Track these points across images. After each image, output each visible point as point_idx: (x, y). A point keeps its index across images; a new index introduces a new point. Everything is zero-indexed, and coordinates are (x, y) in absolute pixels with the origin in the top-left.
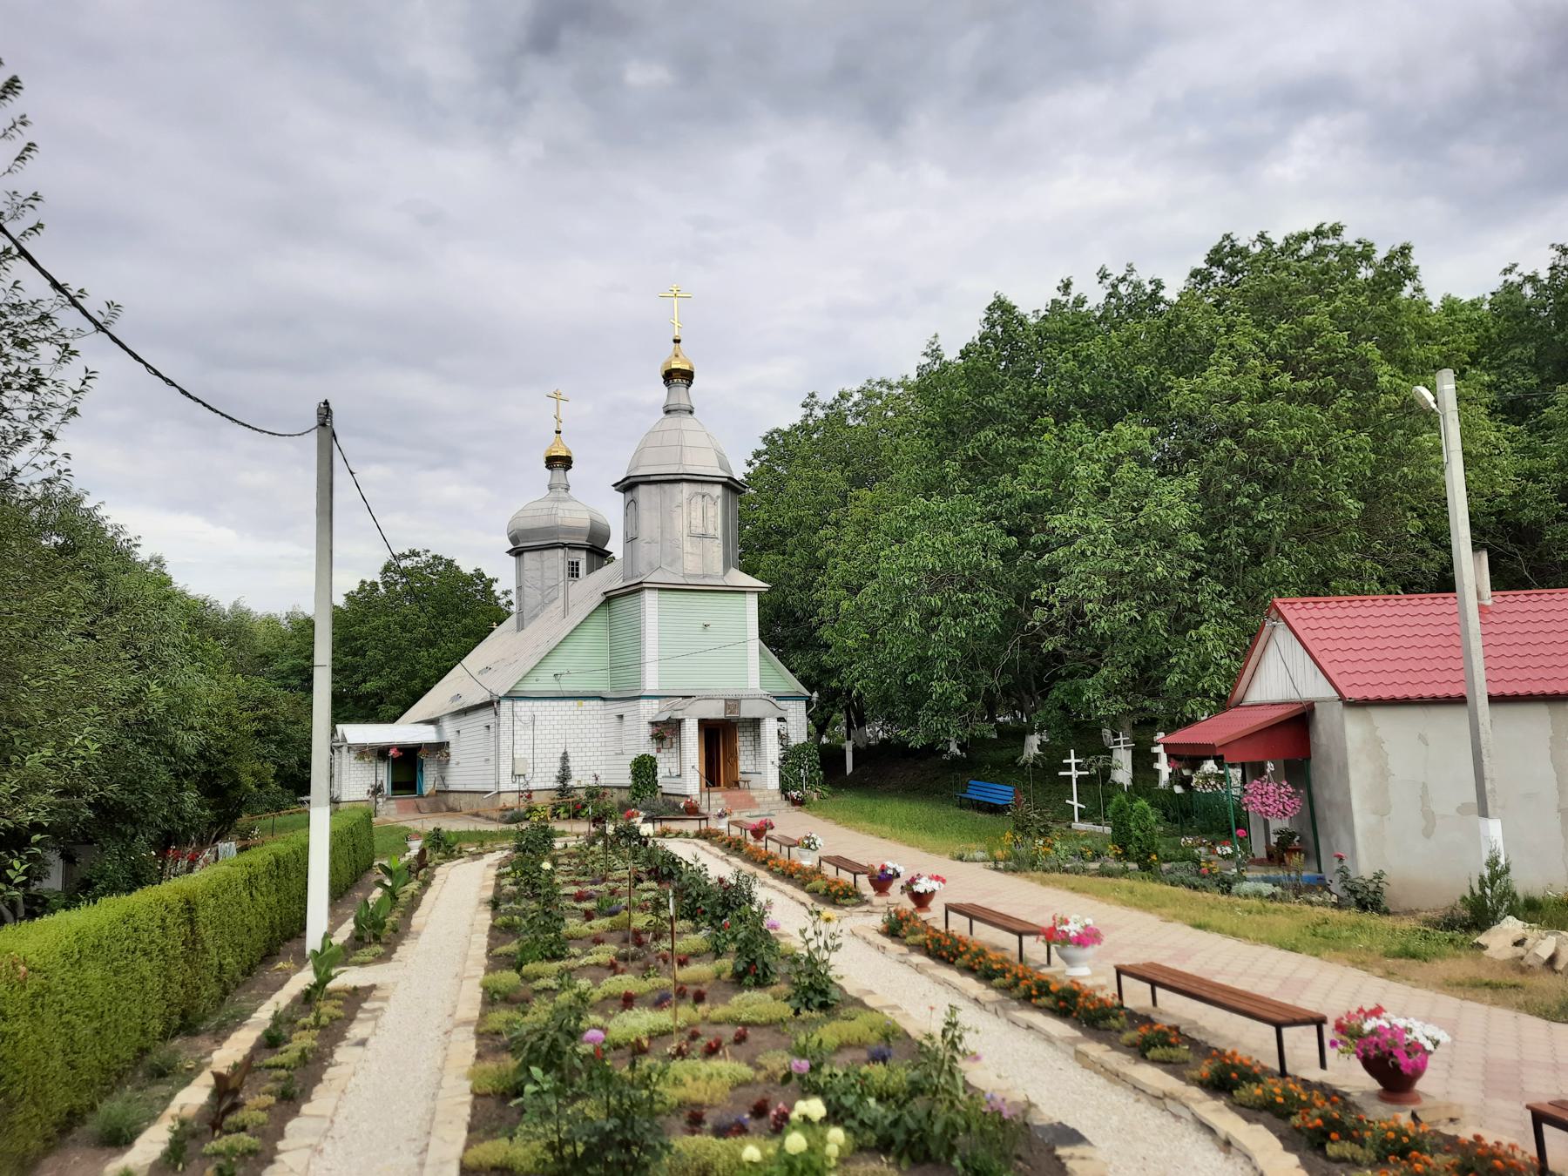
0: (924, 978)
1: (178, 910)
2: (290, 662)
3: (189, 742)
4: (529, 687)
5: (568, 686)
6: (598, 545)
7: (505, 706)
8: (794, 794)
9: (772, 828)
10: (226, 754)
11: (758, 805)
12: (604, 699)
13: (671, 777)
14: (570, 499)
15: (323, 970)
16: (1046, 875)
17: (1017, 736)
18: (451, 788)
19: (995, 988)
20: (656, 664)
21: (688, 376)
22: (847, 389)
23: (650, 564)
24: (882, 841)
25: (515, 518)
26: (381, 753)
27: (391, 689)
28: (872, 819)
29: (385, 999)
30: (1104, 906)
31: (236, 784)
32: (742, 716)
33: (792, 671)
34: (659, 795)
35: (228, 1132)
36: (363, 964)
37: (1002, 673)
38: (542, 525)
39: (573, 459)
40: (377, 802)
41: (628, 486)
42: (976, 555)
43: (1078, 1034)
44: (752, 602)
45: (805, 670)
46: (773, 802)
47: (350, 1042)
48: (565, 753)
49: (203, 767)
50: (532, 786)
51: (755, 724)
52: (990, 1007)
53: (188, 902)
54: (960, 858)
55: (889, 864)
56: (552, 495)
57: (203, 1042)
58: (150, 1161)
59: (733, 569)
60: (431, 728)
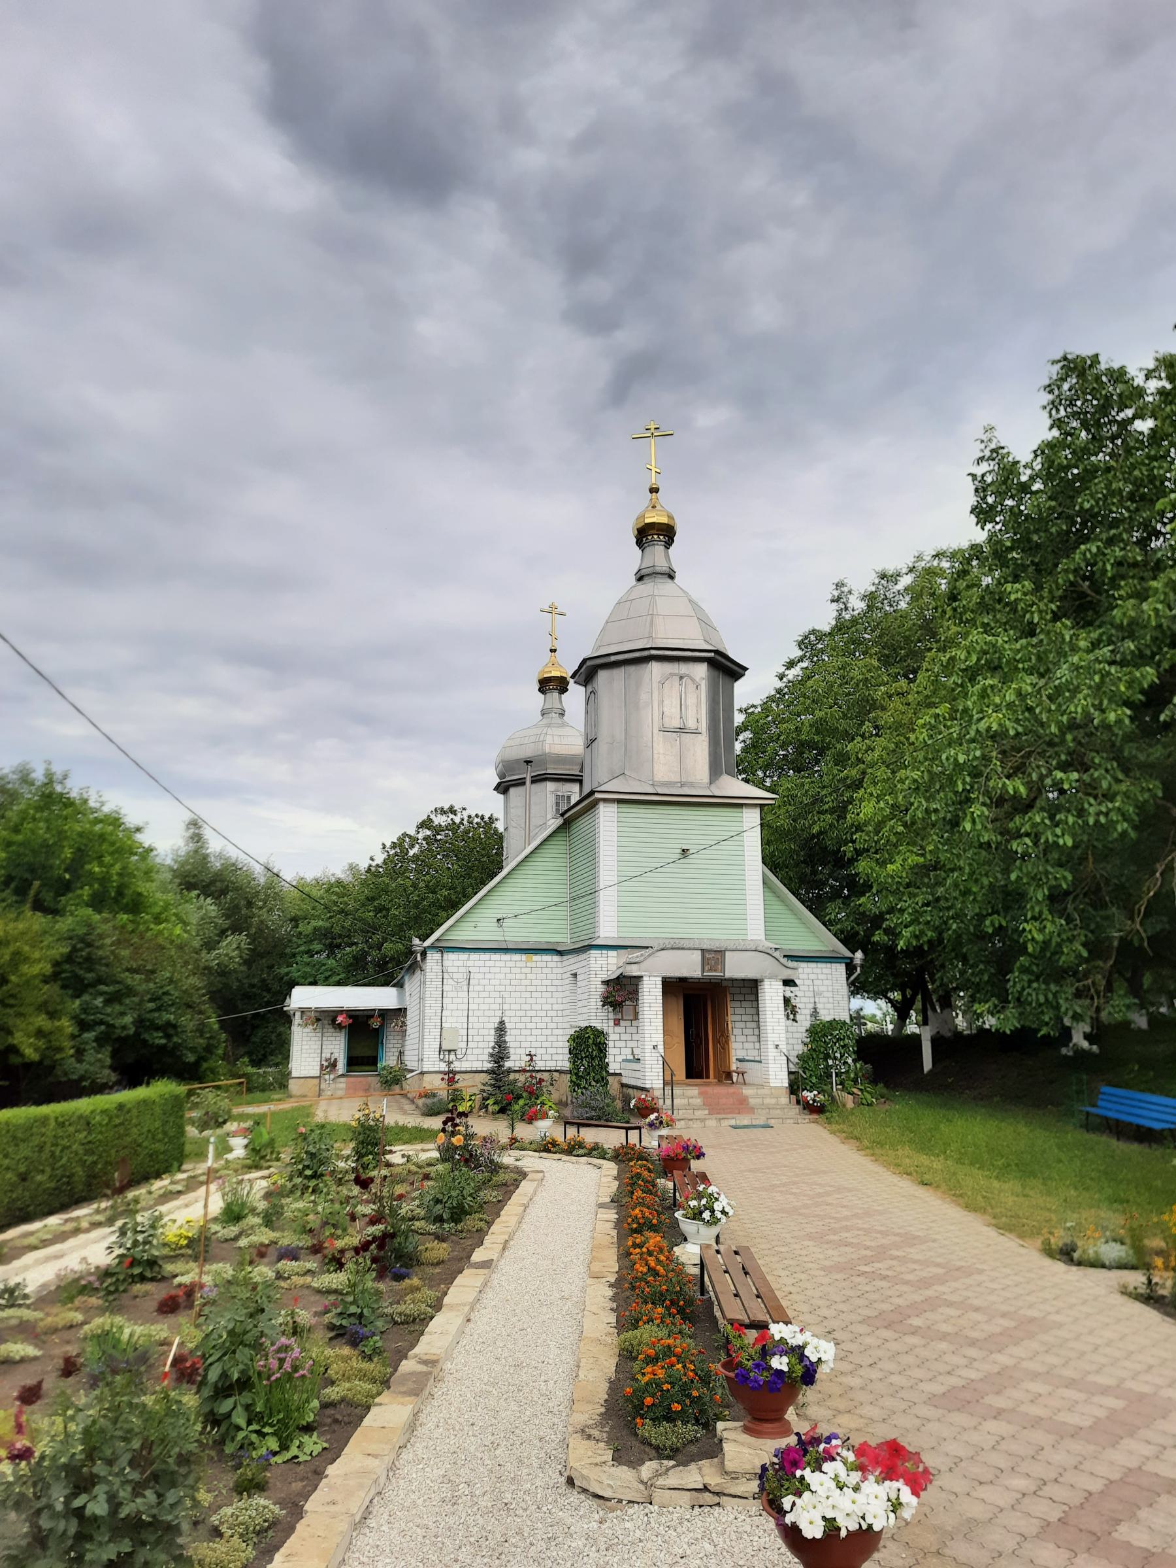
5: (516, 933)
8: (809, 1095)
9: (700, 1155)
11: (751, 1110)
12: (560, 953)
14: (564, 725)
22: (891, 569)
28: (925, 1145)
32: (728, 975)
37: (1148, 914)
42: (1080, 705)
44: (752, 818)
48: (502, 1023)
50: (457, 1066)
51: (750, 988)
54: (1067, 1254)
56: (545, 721)
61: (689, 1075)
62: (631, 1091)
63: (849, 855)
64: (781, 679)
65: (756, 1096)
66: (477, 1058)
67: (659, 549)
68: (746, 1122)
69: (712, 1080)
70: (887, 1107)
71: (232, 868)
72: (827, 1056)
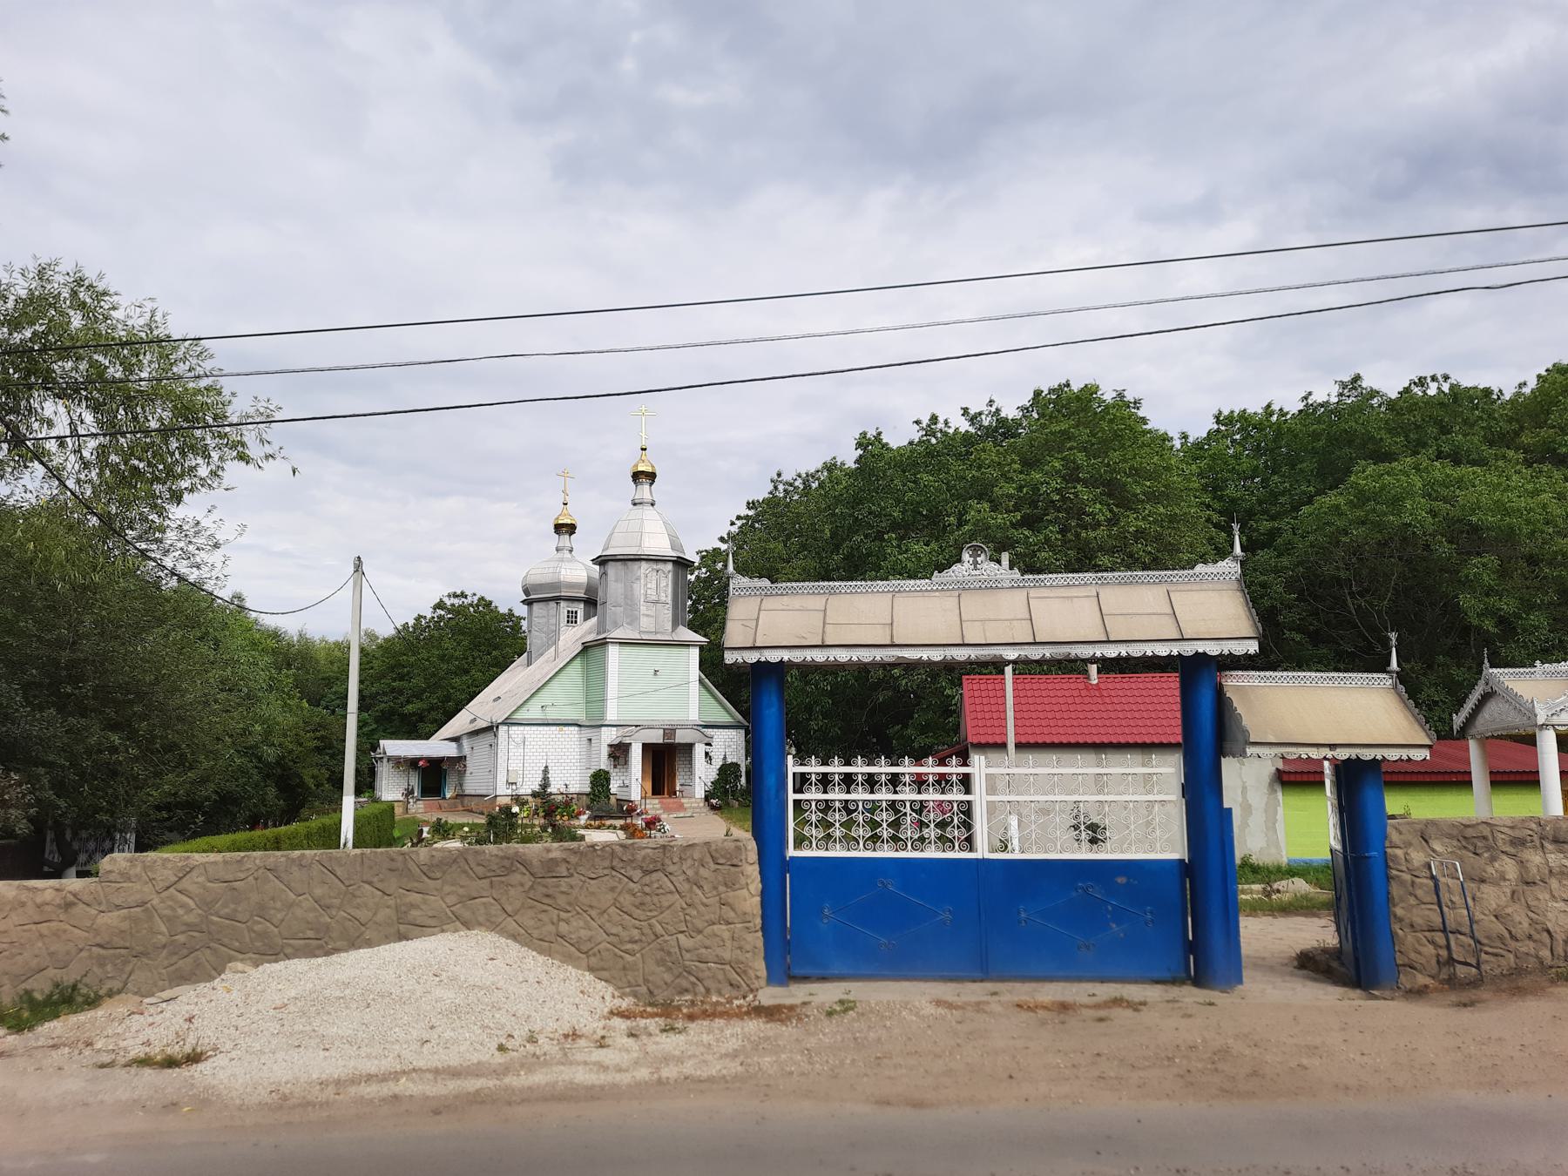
3: (270, 753)
5: (552, 715)
7: (503, 729)
8: (714, 801)
18: (467, 792)
21: (651, 476)
26: (413, 763)
38: (548, 581)
41: (602, 561)
46: (698, 807)
48: (546, 767)
51: (688, 748)
59: (681, 627)
60: (454, 745)
61: (653, 794)
67: (647, 487)
69: (666, 796)
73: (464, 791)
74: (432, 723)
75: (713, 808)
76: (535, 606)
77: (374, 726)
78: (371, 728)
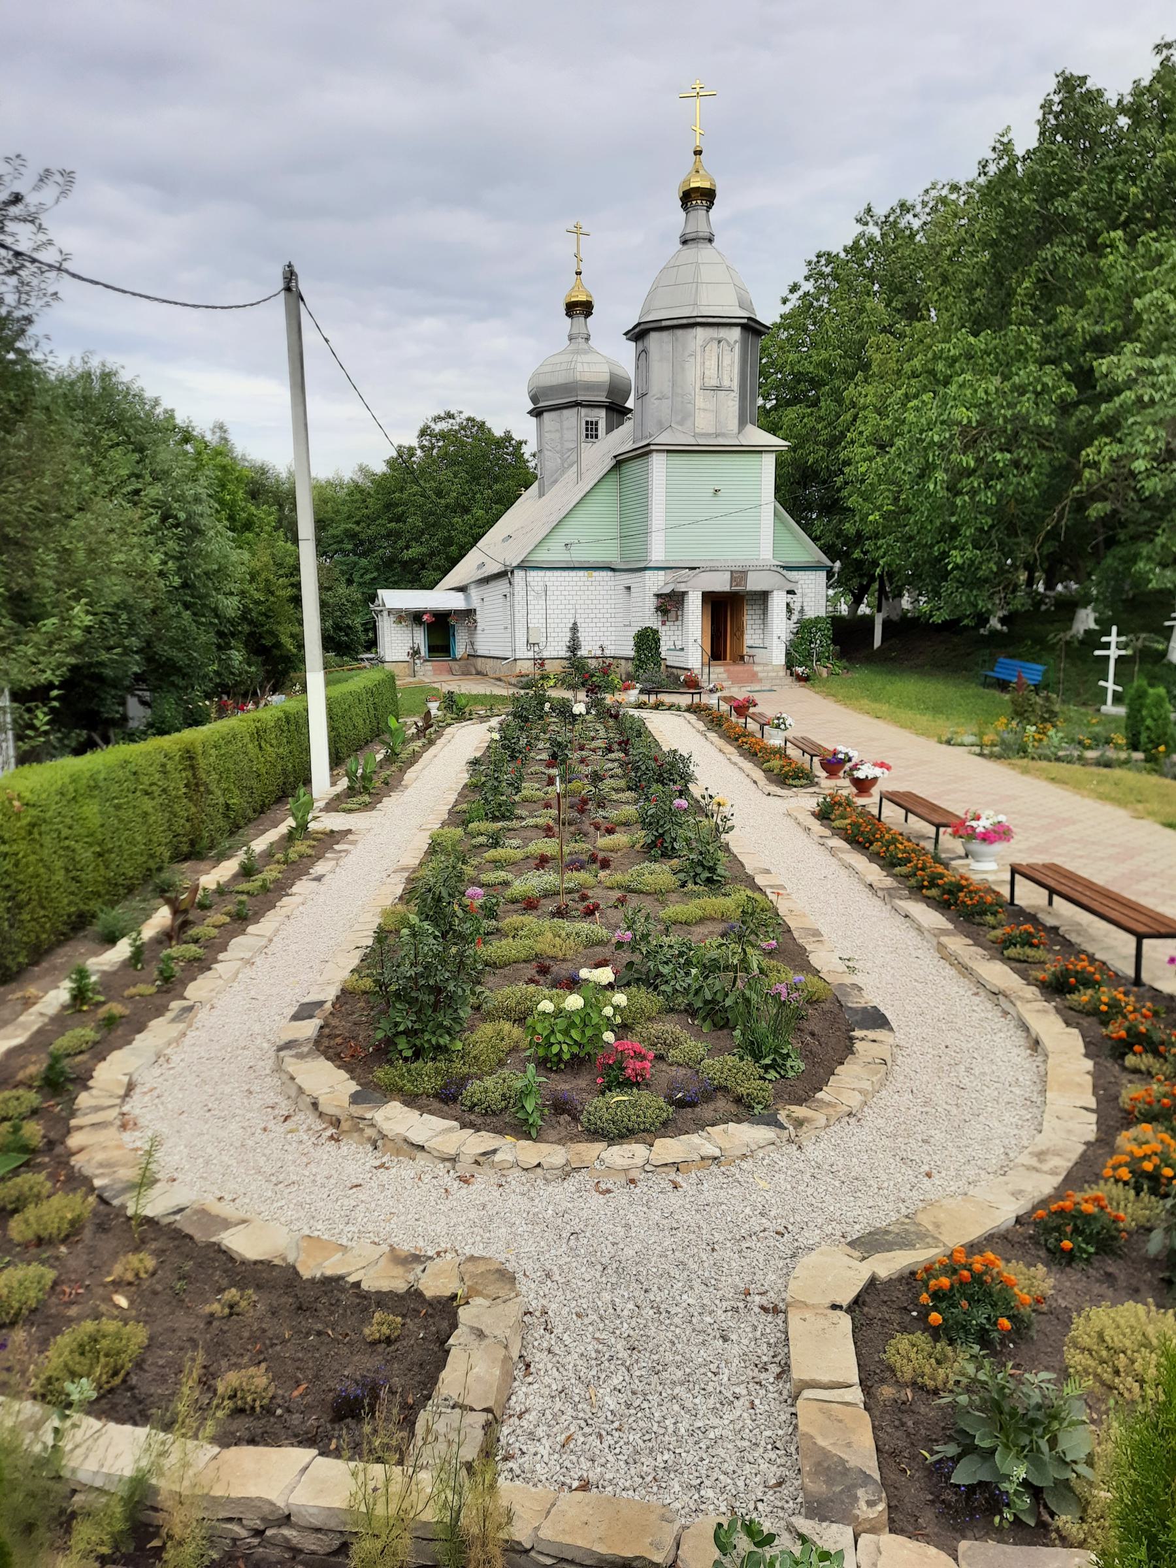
0: (834, 860)
1: (177, 758)
2: (343, 526)
3: (230, 605)
4: (541, 557)
6: (618, 401)
7: (519, 575)
8: (800, 670)
9: (755, 706)
10: (268, 617)
11: (760, 681)
12: (613, 570)
13: (675, 650)
14: (590, 351)
15: (300, 815)
16: (1032, 764)
17: (1068, 608)
18: (480, 653)
19: (895, 876)
20: (662, 533)
23: (660, 423)
24: (876, 721)
25: (536, 374)
26: (416, 617)
27: (432, 555)
28: (876, 699)
29: (353, 843)
30: (1078, 798)
31: (278, 645)
32: (749, 588)
33: (815, 539)
34: (663, 667)
35: (186, 942)
36: (350, 811)
39: (595, 304)
40: (415, 664)
41: (639, 334)
43: (950, 926)
44: (769, 462)
45: (829, 539)
47: (310, 877)
48: (575, 624)
49: (246, 628)
50: (545, 654)
51: (763, 597)
52: (880, 893)
53: (188, 752)
55: (840, 748)
56: (573, 347)
57: (202, 866)
58: (121, 959)
62: (674, 671)
63: (838, 484)
64: (784, 303)
65: (763, 671)
66: (557, 648)
68: (757, 688)
70: (849, 675)
71: (263, 471)
72: (811, 642)
73: (475, 651)
74: (434, 570)
75: (801, 679)
76: (546, 416)
77: (375, 574)
78: (372, 576)
